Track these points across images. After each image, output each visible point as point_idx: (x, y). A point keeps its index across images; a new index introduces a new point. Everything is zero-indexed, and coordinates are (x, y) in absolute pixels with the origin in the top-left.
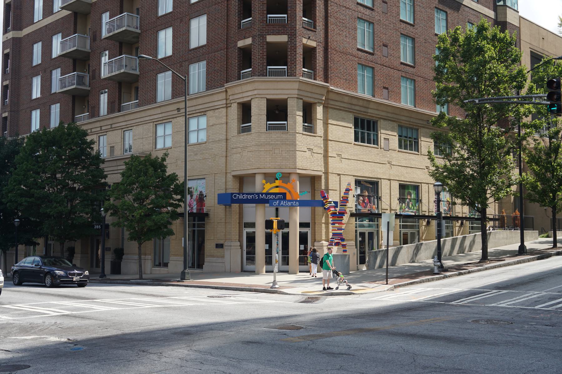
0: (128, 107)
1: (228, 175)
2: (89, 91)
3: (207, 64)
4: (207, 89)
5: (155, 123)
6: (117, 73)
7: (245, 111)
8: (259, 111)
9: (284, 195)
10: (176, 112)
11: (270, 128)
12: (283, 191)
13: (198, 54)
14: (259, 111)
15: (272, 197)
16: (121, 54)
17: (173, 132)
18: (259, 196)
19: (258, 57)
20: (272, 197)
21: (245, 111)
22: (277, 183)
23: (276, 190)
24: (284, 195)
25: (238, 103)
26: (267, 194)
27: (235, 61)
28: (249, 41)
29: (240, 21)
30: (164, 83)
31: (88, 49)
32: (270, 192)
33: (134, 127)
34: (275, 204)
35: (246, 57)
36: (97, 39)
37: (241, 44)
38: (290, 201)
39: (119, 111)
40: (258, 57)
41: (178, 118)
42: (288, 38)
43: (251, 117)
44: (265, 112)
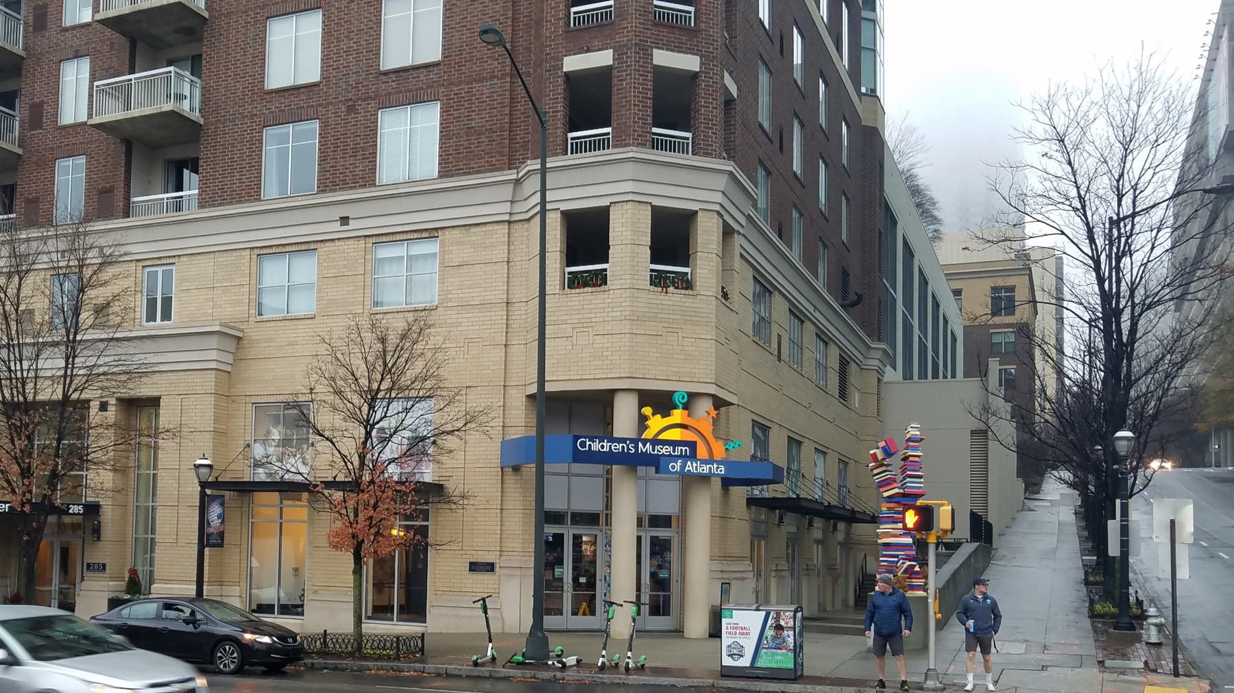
0: (149, 208)
1: (512, 392)
2: (694, 76)
3: (444, 112)
4: (445, 173)
5: (257, 252)
6: (148, 111)
7: (586, 238)
8: (629, 238)
9: (692, 445)
10: (337, 226)
11: (658, 280)
12: (690, 436)
13: (409, 86)
14: (629, 238)
15: (665, 450)
16: (132, 71)
17: (322, 278)
18: (636, 447)
19: (631, 99)
20: (665, 450)
21: (586, 238)
22: (677, 416)
23: (675, 434)
24: (692, 445)
25: (562, 212)
26: (655, 442)
27: (555, 105)
28: (603, 58)
29: (568, 8)
30: (289, 151)
31: (19, 49)
32: (662, 437)
33: (184, 259)
34: (673, 467)
35: (589, 103)
36: (50, 25)
37: (572, 63)
38: (704, 462)
39: (127, 214)
40: (631, 99)
41: (337, 243)
42: (702, 63)
43: (609, 248)
44: (647, 240)
